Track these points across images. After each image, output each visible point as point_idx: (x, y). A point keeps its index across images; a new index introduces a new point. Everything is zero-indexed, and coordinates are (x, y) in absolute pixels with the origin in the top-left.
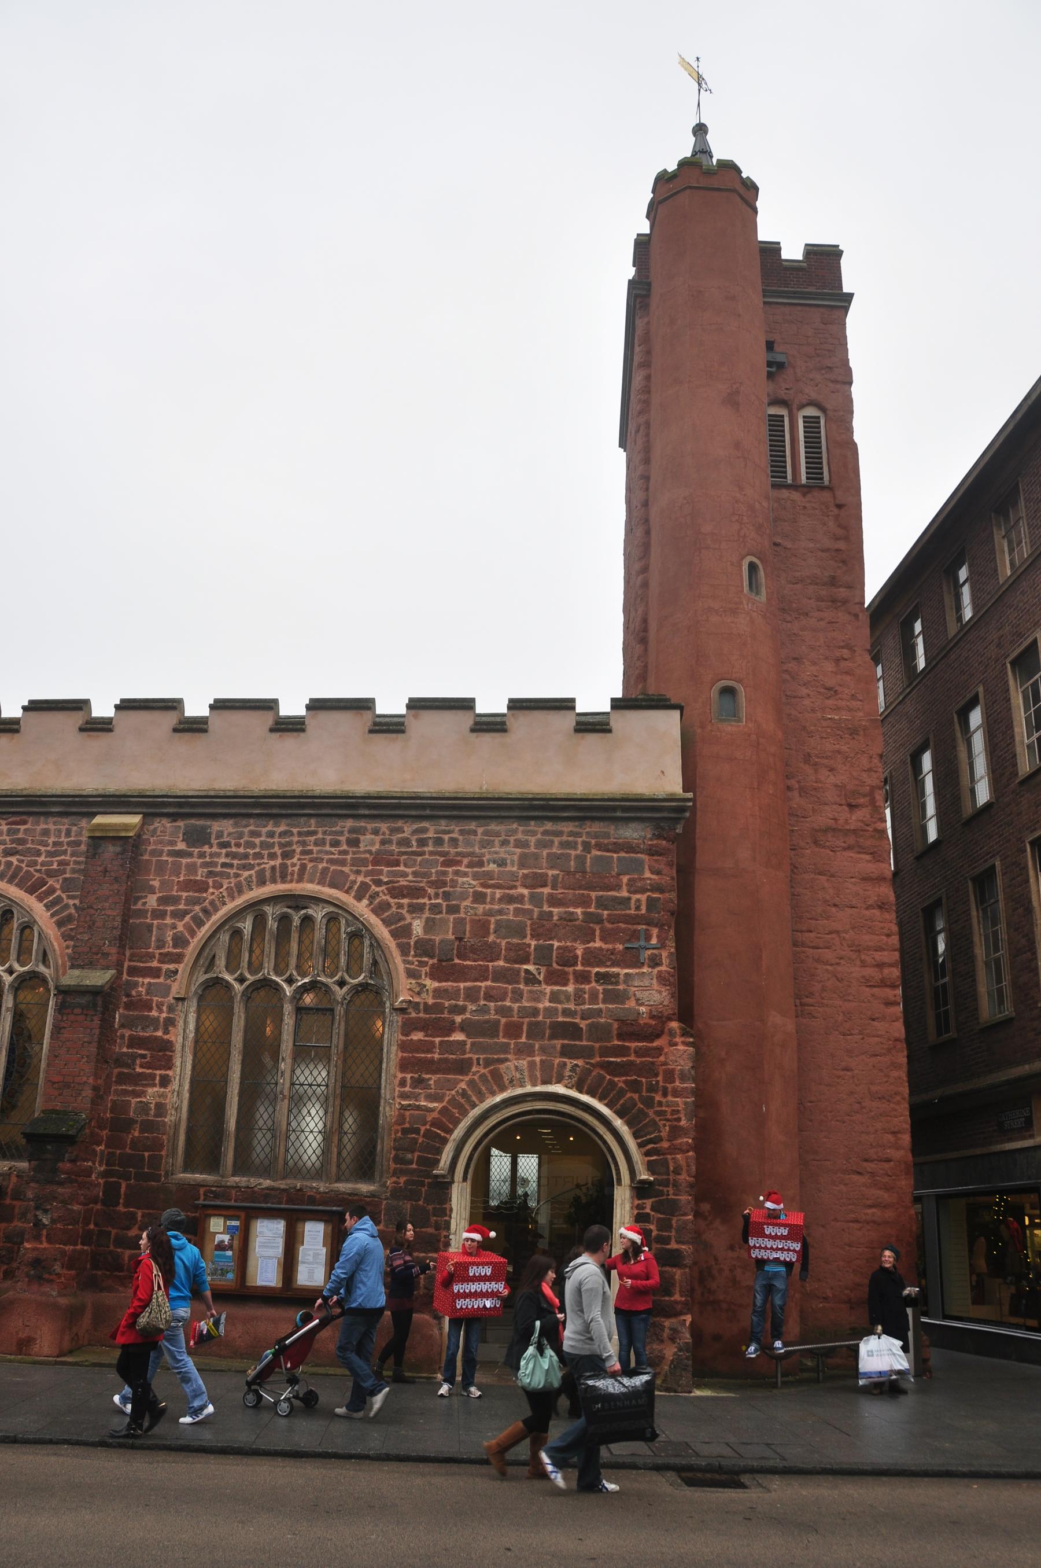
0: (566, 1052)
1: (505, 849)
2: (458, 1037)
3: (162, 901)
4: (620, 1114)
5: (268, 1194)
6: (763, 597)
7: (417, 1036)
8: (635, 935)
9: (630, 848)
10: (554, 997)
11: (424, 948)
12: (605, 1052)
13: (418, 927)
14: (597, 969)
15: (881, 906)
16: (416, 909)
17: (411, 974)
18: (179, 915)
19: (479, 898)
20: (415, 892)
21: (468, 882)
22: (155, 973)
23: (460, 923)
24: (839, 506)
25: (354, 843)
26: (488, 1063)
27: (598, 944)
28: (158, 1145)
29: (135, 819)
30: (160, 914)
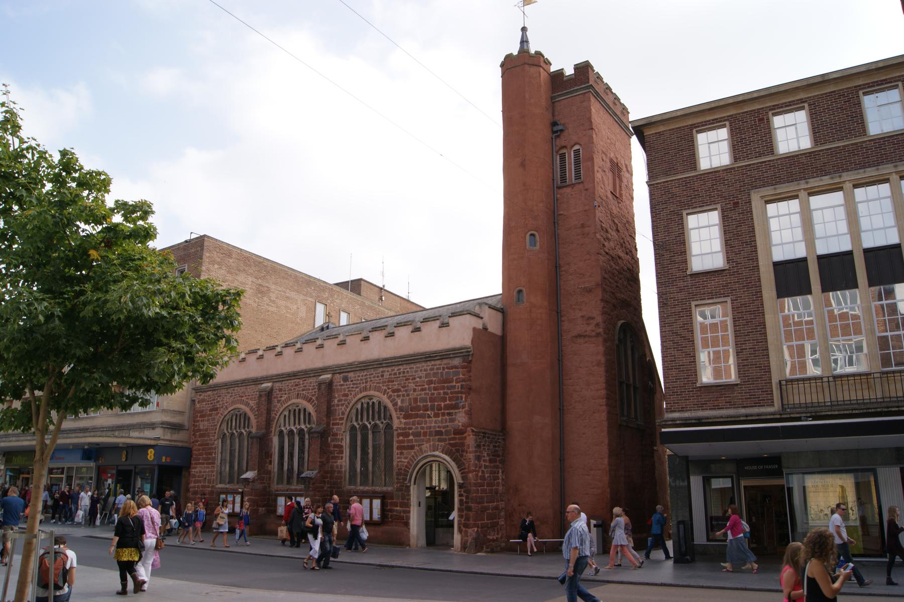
0: (440, 440)
1: (421, 371)
2: (411, 437)
3: (339, 401)
4: (454, 461)
5: (367, 492)
6: (538, 247)
7: (401, 438)
8: (457, 398)
9: (456, 367)
10: (436, 422)
11: (401, 409)
12: (450, 439)
13: (399, 403)
14: (731, 350)
15: (598, 364)
16: (398, 396)
17: (398, 418)
18: (342, 405)
19: (415, 390)
20: (398, 390)
21: (412, 386)
22: (338, 424)
23: (410, 399)
24: (586, 190)
25: (382, 376)
26: (419, 445)
27: (448, 402)
28: (341, 478)
29: (329, 376)
30: (338, 405)
